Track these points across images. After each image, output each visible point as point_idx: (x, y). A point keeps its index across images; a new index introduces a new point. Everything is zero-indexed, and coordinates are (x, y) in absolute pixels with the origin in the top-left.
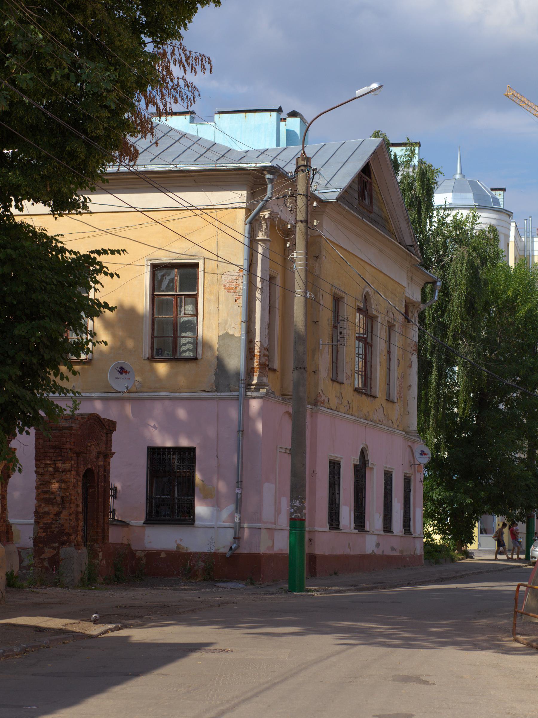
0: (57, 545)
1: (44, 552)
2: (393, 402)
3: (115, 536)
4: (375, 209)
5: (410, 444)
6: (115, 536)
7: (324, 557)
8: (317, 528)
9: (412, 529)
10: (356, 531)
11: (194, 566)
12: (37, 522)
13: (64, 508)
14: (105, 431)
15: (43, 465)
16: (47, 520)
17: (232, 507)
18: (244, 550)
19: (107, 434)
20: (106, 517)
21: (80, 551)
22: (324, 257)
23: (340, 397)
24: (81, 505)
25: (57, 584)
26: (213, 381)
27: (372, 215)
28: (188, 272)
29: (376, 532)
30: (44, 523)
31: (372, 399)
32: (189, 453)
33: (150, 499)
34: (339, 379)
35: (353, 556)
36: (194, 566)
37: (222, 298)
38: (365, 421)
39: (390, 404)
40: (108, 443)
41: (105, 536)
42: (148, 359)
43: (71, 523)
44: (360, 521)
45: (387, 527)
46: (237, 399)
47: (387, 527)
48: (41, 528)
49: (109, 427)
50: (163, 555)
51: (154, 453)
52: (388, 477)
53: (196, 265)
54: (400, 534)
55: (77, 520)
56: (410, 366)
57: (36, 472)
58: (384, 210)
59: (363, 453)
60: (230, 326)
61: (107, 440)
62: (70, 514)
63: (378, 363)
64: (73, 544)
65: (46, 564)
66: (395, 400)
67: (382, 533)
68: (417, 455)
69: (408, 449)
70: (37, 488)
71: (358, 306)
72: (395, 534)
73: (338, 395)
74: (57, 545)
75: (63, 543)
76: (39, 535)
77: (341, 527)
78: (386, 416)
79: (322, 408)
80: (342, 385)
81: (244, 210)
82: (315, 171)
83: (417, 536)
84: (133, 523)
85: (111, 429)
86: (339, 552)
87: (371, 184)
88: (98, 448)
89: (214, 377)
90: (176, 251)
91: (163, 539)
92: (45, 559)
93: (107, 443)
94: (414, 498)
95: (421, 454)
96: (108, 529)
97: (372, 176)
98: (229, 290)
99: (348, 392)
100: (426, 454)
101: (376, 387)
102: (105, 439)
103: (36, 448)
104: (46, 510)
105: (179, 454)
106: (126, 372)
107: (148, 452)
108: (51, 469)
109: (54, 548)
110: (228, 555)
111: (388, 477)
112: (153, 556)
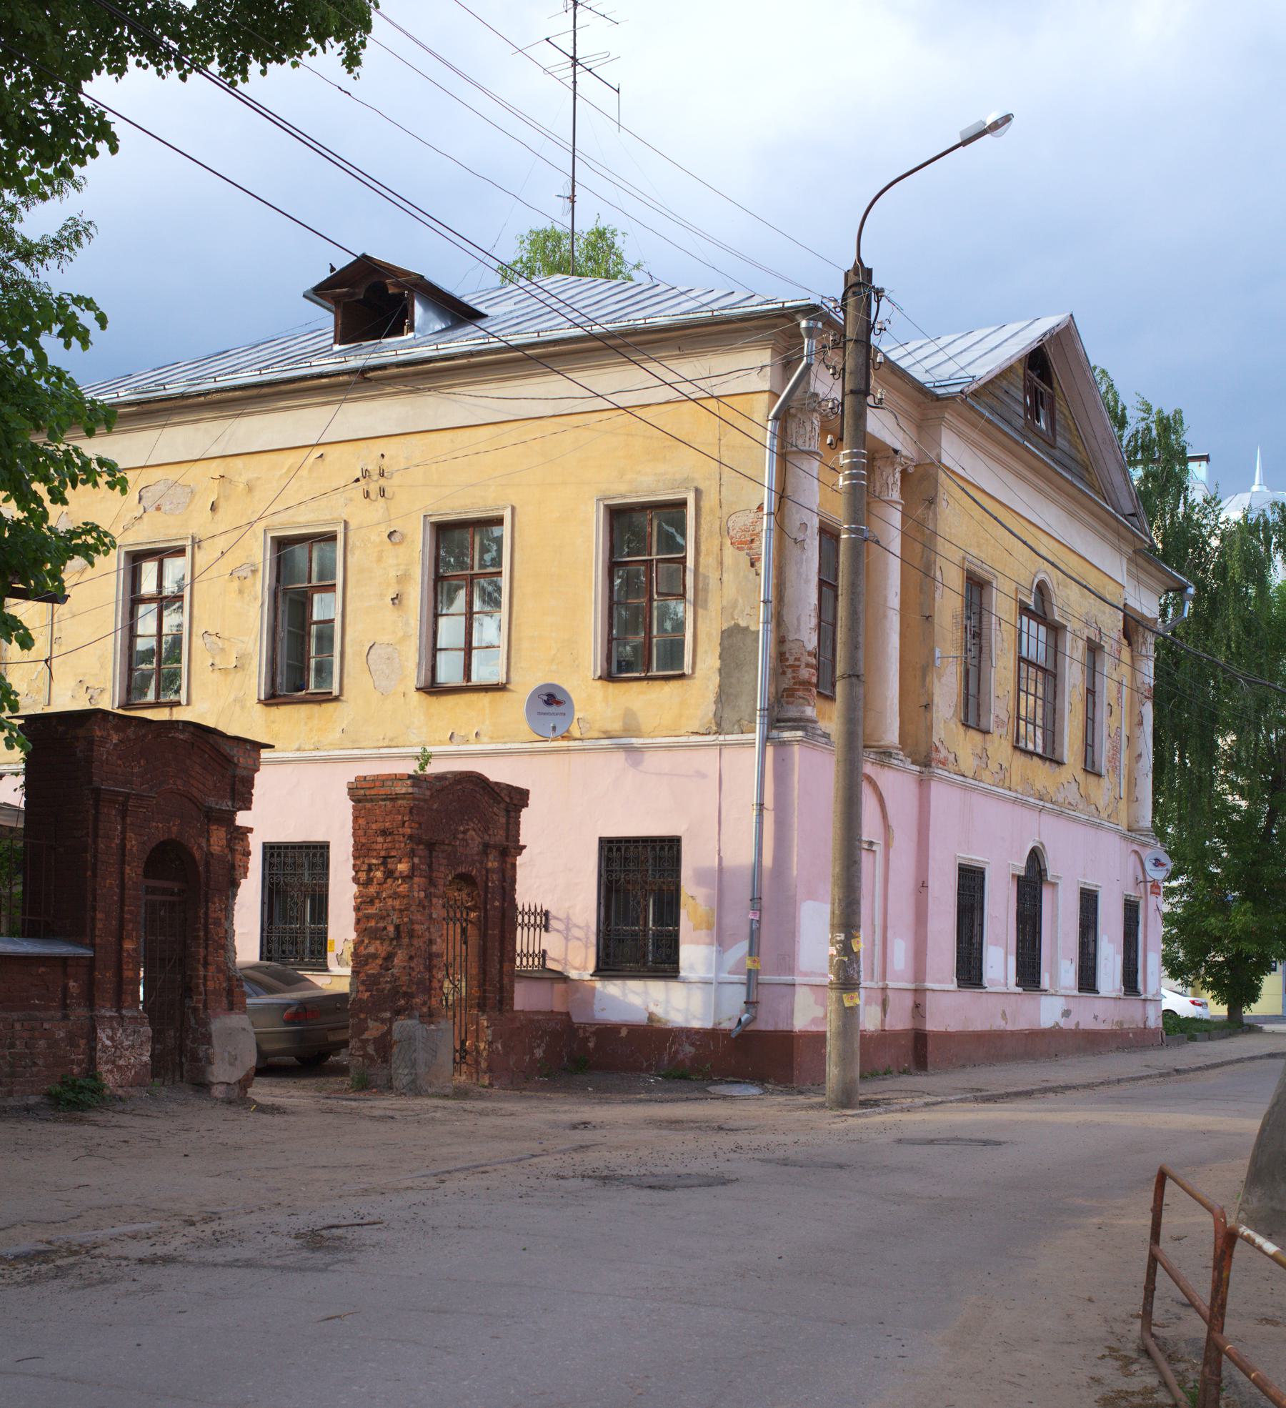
0: (388, 1015)
1: (367, 1029)
2: (1099, 775)
3: (525, 998)
4: (1060, 442)
5: (1136, 847)
7: (947, 1036)
8: (929, 985)
9: (1140, 987)
10: (1020, 990)
11: (676, 1052)
12: (355, 973)
13: (399, 946)
14: (502, 805)
15: (365, 867)
16: (373, 969)
17: (743, 946)
18: (765, 1023)
19: (508, 811)
20: (506, 964)
21: (433, 1027)
22: (944, 503)
23: (983, 756)
25: (389, 1087)
26: (711, 715)
27: (1057, 453)
29: (1063, 992)
30: (368, 976)
31: (1055, 766)
32: (671, 848)
34: (983, 725)
35: (1013, 1033)
36: (676, 1052)
37: (728, 560)
38: (1037, 802)
39: (1092, 779)
42: (600, 678)
43: (414, 974)
44: (1029, 972)
45: (1087, 980)
47: (1087, 980)
48: (363, 983)
50: (624, 1033)
51: (610, 850)
52: (1089, 900)
53: (682, 504)
54: (1114, 995)
56: (1141, 723)
57: (356, 880)
58: (1081, 448)
59: (1035, 857)
60: (742, 611)
61: (508, 823)
62: (411, 958)
63: (1067, 704)
64: (417, 1014)
65: (371, 1050)
66: (1104, 772)
67: (1076, 992)
68: (1149, 865)
69: (1133, 858)
70: (357, 909)
71: (1021, 602)
72: (1103, 992)
73: (979, 751)
74: (388, 1015)
75: (398, 1012)
76: (360, 995)
77: (985, 982)
78: (1086, 798)
79: (940, 771)
80: (988, 737)
81: (766, 396)
82: (879, 293)
83: (1150, 997)
85: (515, 802)
86: (979, 1025)
87: (1052, 398)
88: (487, 837)
89: (713, 707)
90: (645, 482)
91: (634, 999)
92: (368, 1040)
93: (508, 829)
94: (1145, 937)
95: (1155, 865)
96: (512, 986)
97: (1055, 385)
98: (738, 545)
99: (1000, 747)
100: (1163, 865)
101: (1062, 745)
102: (503, 820)
103: (354, 835)
104: (372, 949)
105: (653, 848)
106: (559, 703)
107: (601, 848)
108: (379, 874)
109: (383, 1021)
111: (1089, 900)
112: (608, 1032)
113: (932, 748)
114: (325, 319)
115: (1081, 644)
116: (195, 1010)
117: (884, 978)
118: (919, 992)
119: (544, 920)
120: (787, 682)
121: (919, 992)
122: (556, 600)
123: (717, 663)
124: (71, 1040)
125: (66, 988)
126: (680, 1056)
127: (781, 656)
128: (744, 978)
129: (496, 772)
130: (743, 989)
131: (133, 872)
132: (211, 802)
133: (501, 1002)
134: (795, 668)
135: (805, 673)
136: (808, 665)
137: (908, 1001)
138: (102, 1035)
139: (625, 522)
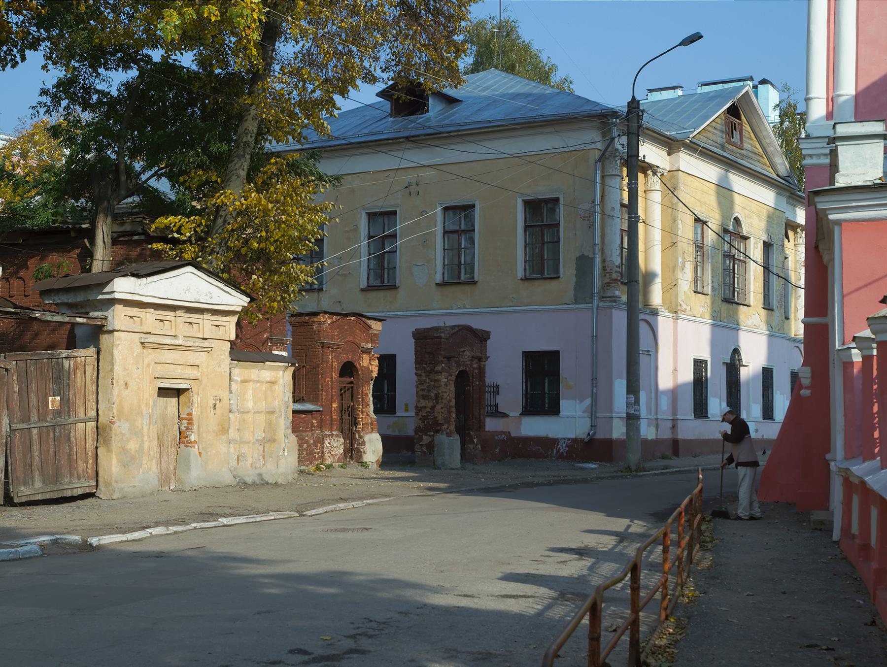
6: (491, 425)
8: (679, 417)
12: (417, 415)
18: (600, 436)
24: (454, 401)
28: (467, 209)
33: (526, 395)
40: (484, 349)
41: (481, 425)
46: (592, 309)
49: (482, 337)
55: (450, 412)
75: (437, 432)
77: (709, 415)
82: (643, 111)
84: (511, 414)
90: (542, 191)
91: (536, 427)
104: (423, 405)
110: (586, 440)
113: (677, 304)
114: (387, 106)
115: (760, 246)
116: (359, 432)
117: (657, 414)
118: (675, 421)
119: (496, 390)
120: (607, 280)
121: (675, 421)
122: (503, 241)
123: (575, 272)
124: (315, 444)
125: (312, 423)
126: (561, 450)
127: (604, 268)
128: (589, 415)
129: (477, 324)
130: (589, 420)
131: (335, 375)
132: (363, 345)
133: (480, 427)
134: (610, 273)
135: (615, 276)
136: (616, 272)
137: (670, 424)
138: (326, 442)
139: (533, 206)
